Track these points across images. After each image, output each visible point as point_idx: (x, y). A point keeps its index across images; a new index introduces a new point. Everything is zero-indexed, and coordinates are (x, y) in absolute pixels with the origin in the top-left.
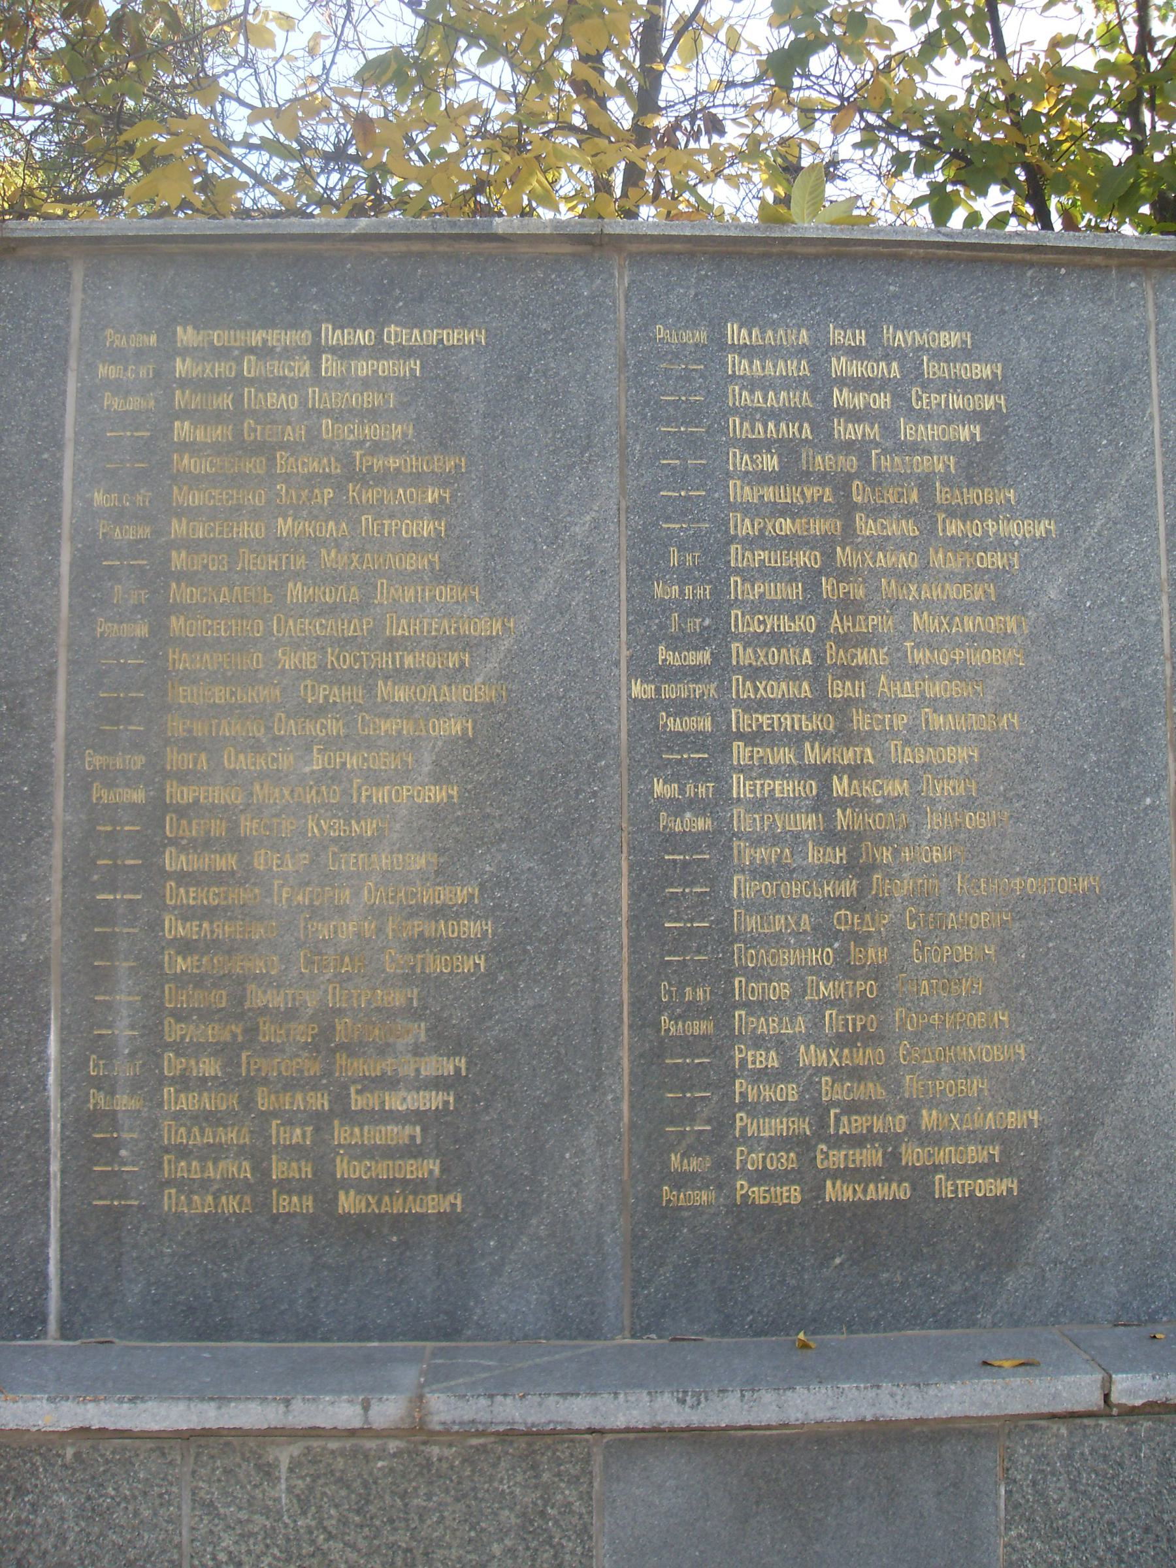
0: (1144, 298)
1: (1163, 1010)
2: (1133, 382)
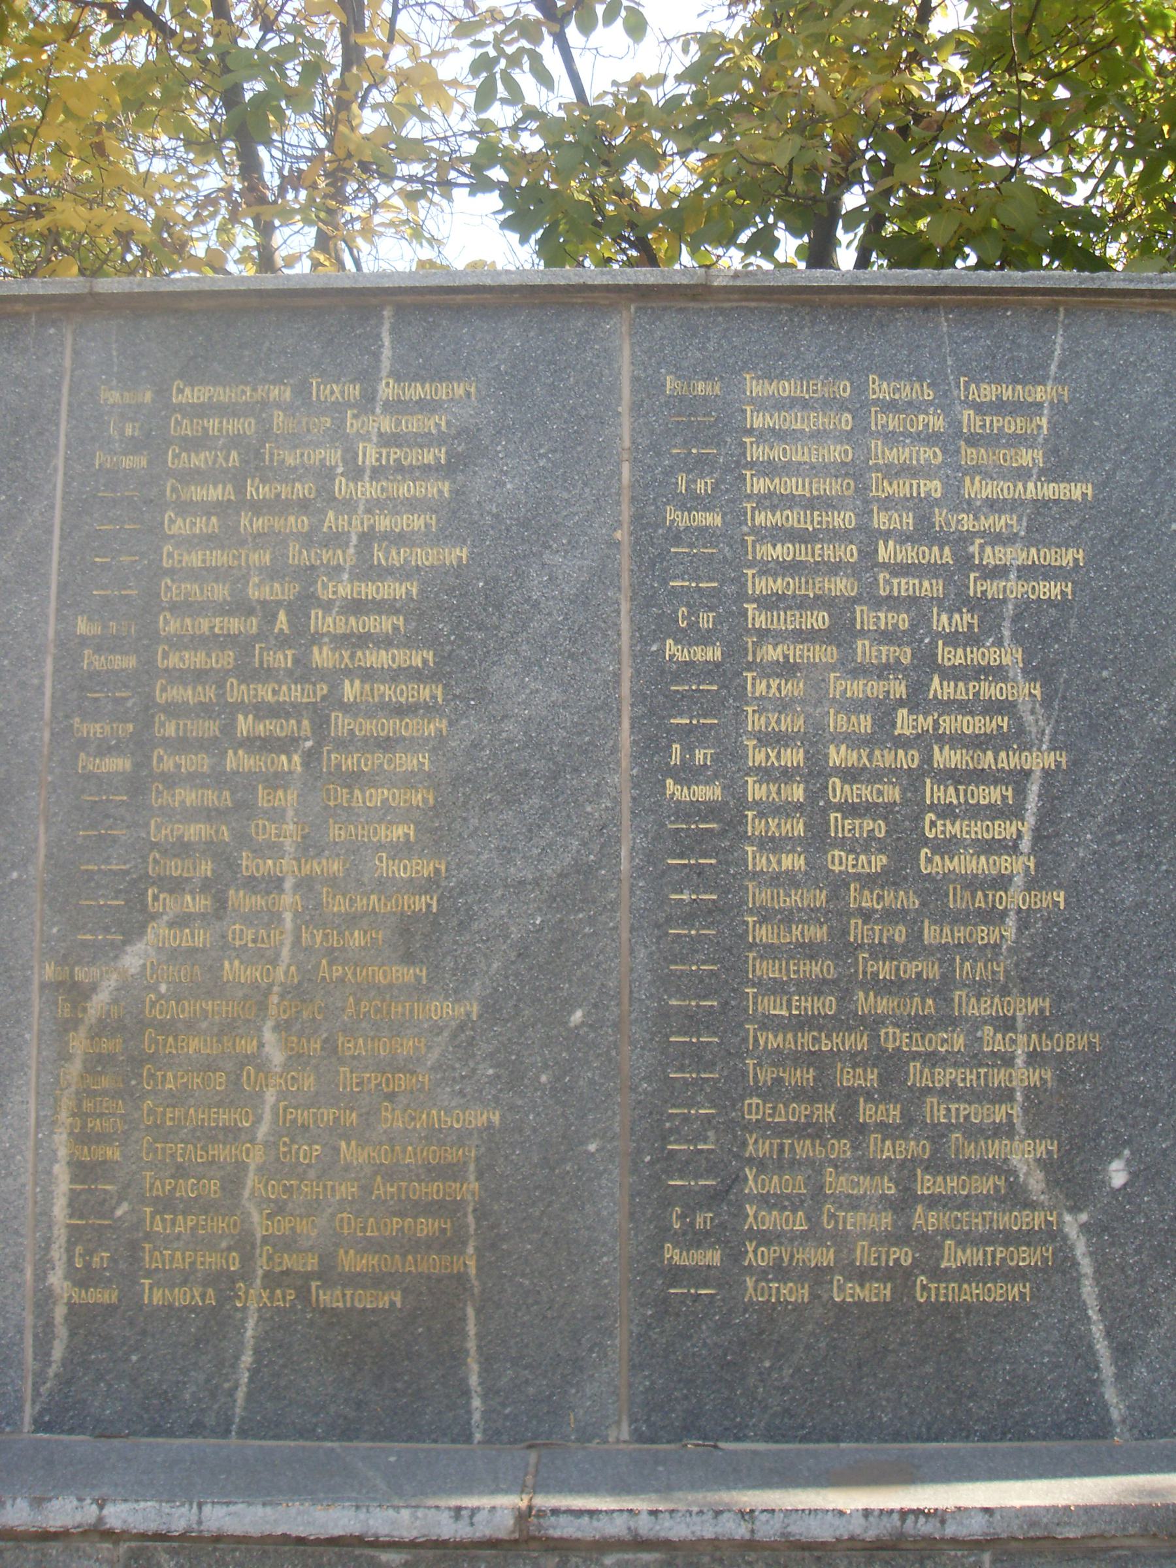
0: (62, 345)
1: (18, 1098)
2: (41, 434)
